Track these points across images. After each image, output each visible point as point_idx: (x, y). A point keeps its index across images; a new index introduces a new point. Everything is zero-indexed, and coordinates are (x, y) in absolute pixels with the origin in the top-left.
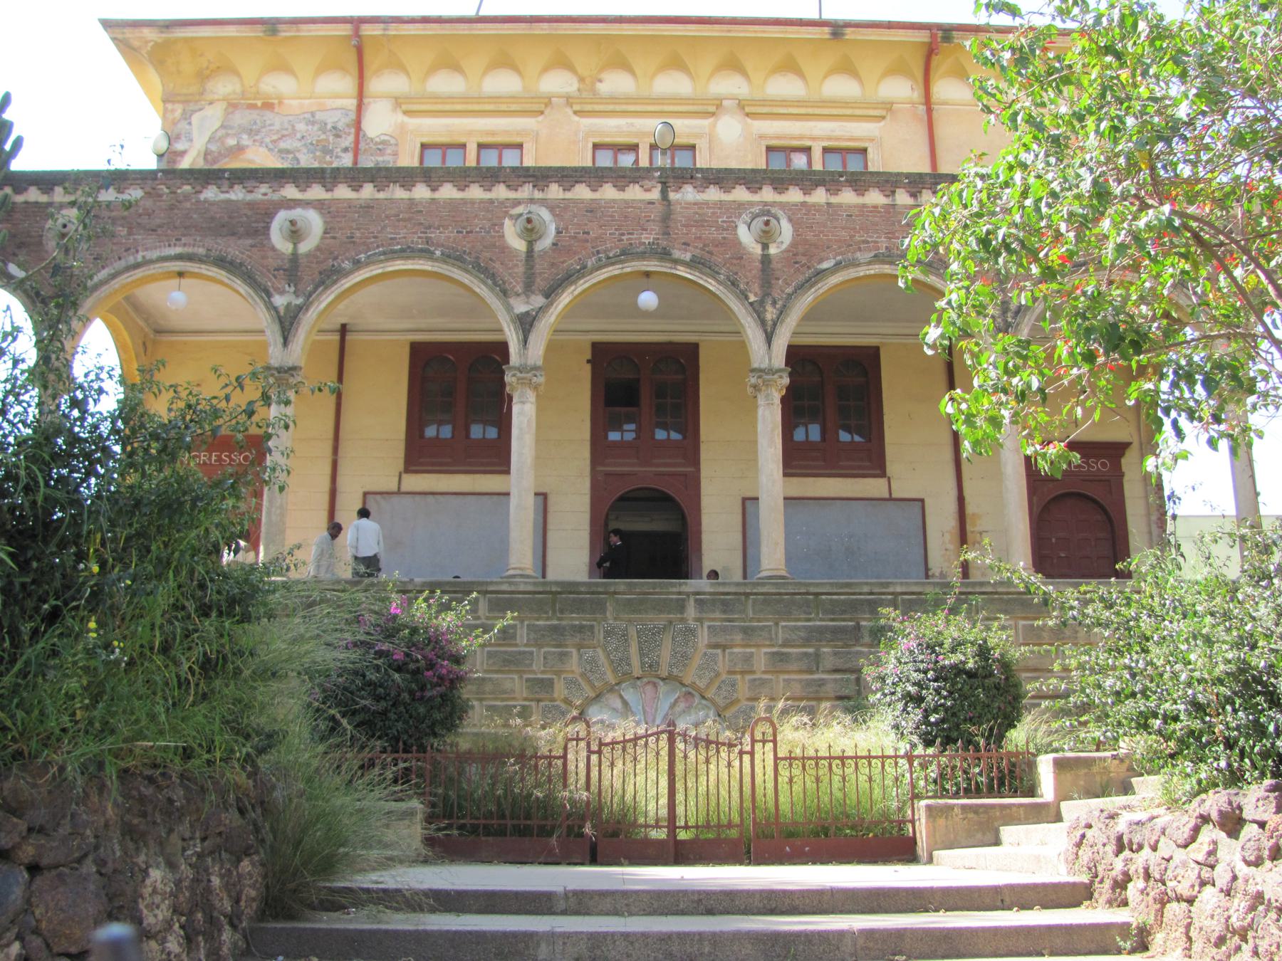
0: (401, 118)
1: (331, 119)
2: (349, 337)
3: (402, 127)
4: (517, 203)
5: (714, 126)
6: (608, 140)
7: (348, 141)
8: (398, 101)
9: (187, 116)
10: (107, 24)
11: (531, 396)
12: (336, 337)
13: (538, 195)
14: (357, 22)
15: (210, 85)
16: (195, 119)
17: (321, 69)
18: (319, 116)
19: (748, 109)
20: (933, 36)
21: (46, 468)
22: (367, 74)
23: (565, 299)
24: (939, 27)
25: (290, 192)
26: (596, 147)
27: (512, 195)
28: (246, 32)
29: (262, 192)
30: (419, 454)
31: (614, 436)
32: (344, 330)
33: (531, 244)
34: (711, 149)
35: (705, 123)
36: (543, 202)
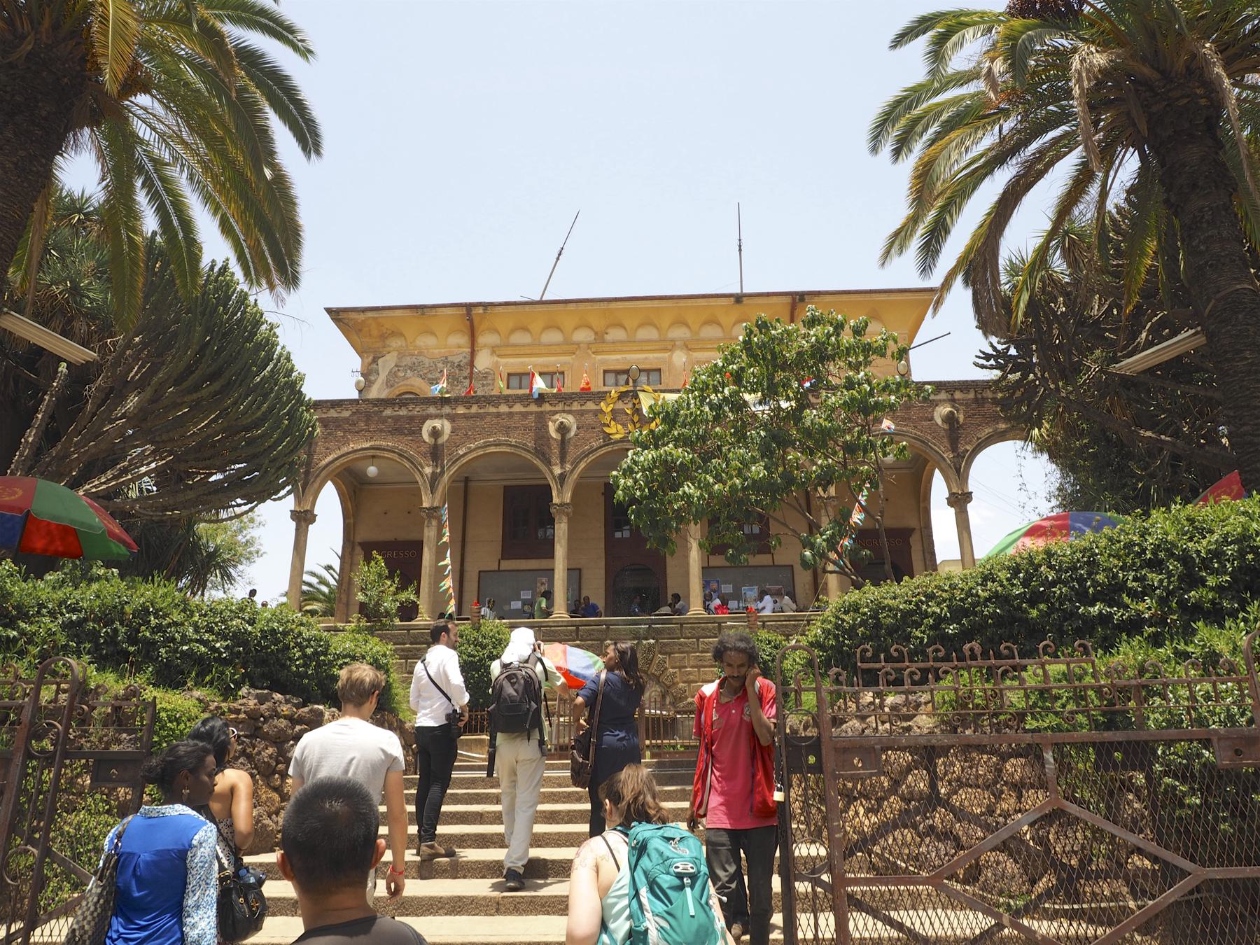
0: (496, 358)
1: (456, 360)
2: (471, 484)
3: (497, 365)
4: (555, 413)
5: (671, 357)
6: (612, 368)
7: (466, 373)
8: (494, 350)
9: (375, 360)
10: (329, 311)
11: (565, 519)
12: (462, 484)
13: (567, 408)
14: (469, 307)
15: (388, 342)
16: (380, 361)
17: (452, 332)
18: (450, 359)
19: (687, 347)
20: (794, 300)
21: (965, 706)
22: (477, 334)
23: (582, 465)
24: (797, 293)
25: (432, 410)
26: (605, 372)
27: (553, 409)
28: (407, 313)
29: (417, 411)
30: (508, 551)
31: (618, 535)
32: (467, 480)
33: (563, 436)
34: (669, 371)
35: (666, 355)
36: (569, 412)
